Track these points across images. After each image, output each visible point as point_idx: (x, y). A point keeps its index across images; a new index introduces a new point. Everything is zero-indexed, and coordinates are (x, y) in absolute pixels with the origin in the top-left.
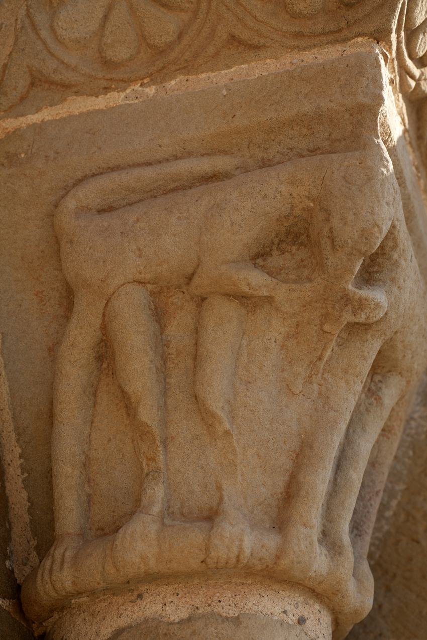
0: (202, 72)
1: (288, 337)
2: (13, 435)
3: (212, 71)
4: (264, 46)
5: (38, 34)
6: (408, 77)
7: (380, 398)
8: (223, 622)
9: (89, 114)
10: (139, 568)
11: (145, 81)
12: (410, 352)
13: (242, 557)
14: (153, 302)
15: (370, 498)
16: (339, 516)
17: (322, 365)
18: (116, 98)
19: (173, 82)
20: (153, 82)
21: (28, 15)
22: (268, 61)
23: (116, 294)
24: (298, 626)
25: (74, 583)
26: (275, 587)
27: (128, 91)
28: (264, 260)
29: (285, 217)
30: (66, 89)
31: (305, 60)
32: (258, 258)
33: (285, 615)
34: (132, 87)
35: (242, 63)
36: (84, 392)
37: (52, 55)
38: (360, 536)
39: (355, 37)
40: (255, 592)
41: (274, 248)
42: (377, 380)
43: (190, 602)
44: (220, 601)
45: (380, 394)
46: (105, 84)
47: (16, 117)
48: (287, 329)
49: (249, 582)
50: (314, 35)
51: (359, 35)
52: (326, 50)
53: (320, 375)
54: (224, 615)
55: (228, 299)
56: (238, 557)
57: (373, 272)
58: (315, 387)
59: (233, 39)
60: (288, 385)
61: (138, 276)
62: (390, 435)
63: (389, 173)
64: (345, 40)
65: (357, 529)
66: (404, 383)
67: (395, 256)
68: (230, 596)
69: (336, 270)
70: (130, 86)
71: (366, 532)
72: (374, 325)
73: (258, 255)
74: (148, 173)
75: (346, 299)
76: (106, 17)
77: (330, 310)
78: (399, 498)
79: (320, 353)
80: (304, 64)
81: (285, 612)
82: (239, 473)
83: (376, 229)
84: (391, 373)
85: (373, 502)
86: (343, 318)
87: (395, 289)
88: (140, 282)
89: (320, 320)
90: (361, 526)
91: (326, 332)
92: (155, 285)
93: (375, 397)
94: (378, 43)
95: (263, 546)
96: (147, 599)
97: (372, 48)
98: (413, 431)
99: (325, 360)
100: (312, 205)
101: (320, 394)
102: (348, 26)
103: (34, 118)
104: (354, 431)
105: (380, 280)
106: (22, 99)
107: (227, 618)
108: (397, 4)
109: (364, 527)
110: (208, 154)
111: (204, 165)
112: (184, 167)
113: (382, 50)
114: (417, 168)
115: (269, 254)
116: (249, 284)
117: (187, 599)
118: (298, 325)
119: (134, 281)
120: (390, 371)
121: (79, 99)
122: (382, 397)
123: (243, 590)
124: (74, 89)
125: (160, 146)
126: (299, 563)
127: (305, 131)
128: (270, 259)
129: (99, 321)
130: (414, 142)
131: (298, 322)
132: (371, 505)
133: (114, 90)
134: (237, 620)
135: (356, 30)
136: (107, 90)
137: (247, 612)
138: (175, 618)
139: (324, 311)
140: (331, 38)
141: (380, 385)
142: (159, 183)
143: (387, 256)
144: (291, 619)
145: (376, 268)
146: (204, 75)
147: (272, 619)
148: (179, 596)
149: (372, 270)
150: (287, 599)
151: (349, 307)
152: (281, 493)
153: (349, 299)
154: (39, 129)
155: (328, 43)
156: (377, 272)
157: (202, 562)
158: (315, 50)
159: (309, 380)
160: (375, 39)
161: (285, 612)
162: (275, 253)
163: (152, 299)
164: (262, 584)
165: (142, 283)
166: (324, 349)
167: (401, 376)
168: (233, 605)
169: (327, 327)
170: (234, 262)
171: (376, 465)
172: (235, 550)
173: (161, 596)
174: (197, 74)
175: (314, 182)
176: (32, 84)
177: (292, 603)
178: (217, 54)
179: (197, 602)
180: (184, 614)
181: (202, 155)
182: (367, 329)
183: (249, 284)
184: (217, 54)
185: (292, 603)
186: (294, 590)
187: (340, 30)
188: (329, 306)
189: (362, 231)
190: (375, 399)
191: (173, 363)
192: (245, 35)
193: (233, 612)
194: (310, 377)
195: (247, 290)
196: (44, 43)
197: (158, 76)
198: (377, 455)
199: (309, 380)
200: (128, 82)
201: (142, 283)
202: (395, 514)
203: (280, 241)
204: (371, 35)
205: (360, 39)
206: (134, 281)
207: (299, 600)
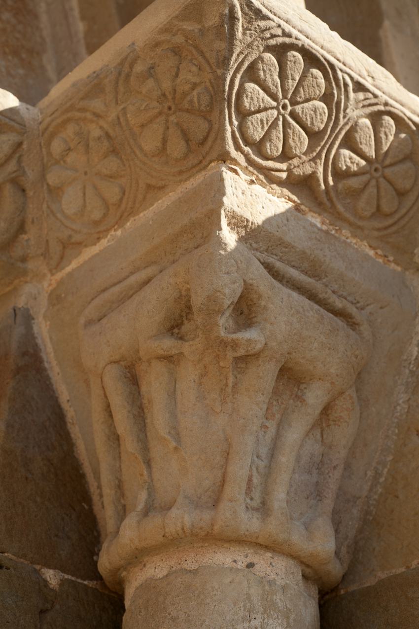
0: (141, 213)
1: (202, 376)
2: (92, 475)
3: (145, 210)
4: (165, 185)
6: (273, 173)
7: (305, 401)
8: (187, 573)
9: (90, 259)
10: (131, 547)
11: (116, 227)
13: (185, 529)
14: (128, 372)
15: (329, 472)
17: (229, 389)
18: (104, 243)
19: (128, 224)
20: (120, 227)
21: (48, 207)
22: (170, 194)
23: (104, 373)
24: (247, 569)
25: (110, 563)
26: (226, 545)
27: (109, 236)
28: (179, 329)
29: (178, 298)
30: (80, 245)
31: (188, 188)
32: (174, 328)
34: (110, 233)
35: (158, 201)
36: (109, 439)
37: (67, 227)
38: (321, 500)
39: (209, 164)
40: (211, 551)
41: (184, 319)
42: (303, 388)
43: (169, 564)
44: (186, 561)
45: (304, 397)
48: (199, 371)
49: (206, 545)
50: (188, 170)
51: (211, 162)
52: (197, 177)
54: (189, 569)
55: (160, 361)
56: (183, 529)
59: (149, 187)
60: (212, 408)
62: (339, 424)
63: (227, 253)
64: (205, 167)
65: (319, 496)
67: (263, 303)
68: (193, 556)
69: (205, 327)
70: (109, 233)
73: (173, 327)
74: (116, 289)
75: (224, 344)
76: (84, 194)
78: (388, 466)
79: (225, 382)
80: (187, 190)
81: (235, 561)
83: (218, 294)
84: (313, 380)
86: (228, 356)
87: (268, 325)
88: (115, 362)
89: (217, 360)
91: (223, 367)
92: (126, 362)
93: (300, 400)
94: (225, 162)
95: (201, 520)
96: (148, 566)
97: (219, 167)
98: (399, 414)
102: (204, 158)
103: (69, 269)
104: (283, 428)
105: (257, 322)
106: (62, 258)
107: (190, 571)
108: (224, 135)
110: (147, 267)
111: (142, 275)
112: (133, 279)
113: (228, 166)
115: (182, 323)
116: (162, 349)
117: (167, 562)
118: (205, 367)
119: (111, 362)
120: (311, 379)
121: (87, 249)
122: (306, 399)
123: (203, 551)
125: (122, 269)
126: (227, 526)
127: (190, 236)
128: (183, 327)
131: (204, 365)
132: (330, 477)
133: (102, 238)
134: (195, 572)
135: (208, 159)
136: (99, 239)
137: (205, 564)
138: (160, 576)
139: (215, 354)
140: (197, 168)
141: (305, 391)
142: (124, 293)
143: (257, 305)
144: (241, 565)
145: (253, 315)
146: (142, 215)
148: (164, 561)
149: (251, 316)
150: (237, 552)
151: (229, 348)
152: (221, 482)
154: (70, 275)
155: (197, 172)
156: (255, 317)
157: (164, 536)
158: (192, 180)
160: (222, 160)
161: (235, 561)
162: (186, 322)
163: (128, 370)
164: (216, 545)
165: (117, 362)
167: (322, 380)
168: (195, 562)
169: (222, 364)
170: (154, 336)
171: (332, 447)
172: (179, 524)
173: (154, 563)
174: (138, 215)
175: (185, 271)
176: (64, 247)
177: (242, 554)
178: (144, 198)
179: (172, 563)
180: (165, 573)
181: (145, 268)
182: (257, 358)
183: (162, 349)
184: (144, 198)
185: (242, 554)
186: (243, 546)
187: (201, 162)
189: (208, 297)
190: (301, 402)
191: (148, 409)
192: (153, 182)
193: (194, 566)
195: (163, 353)
196: (61, 221)
197: (120, 222)
198: (332, 440)
200: (107, 231)
201: (117, 362)
202: (386, 479)
203: (187, 313)
204: (218, 160)
205: (213, 164)
206: (111, 362)
207: (249, 552)
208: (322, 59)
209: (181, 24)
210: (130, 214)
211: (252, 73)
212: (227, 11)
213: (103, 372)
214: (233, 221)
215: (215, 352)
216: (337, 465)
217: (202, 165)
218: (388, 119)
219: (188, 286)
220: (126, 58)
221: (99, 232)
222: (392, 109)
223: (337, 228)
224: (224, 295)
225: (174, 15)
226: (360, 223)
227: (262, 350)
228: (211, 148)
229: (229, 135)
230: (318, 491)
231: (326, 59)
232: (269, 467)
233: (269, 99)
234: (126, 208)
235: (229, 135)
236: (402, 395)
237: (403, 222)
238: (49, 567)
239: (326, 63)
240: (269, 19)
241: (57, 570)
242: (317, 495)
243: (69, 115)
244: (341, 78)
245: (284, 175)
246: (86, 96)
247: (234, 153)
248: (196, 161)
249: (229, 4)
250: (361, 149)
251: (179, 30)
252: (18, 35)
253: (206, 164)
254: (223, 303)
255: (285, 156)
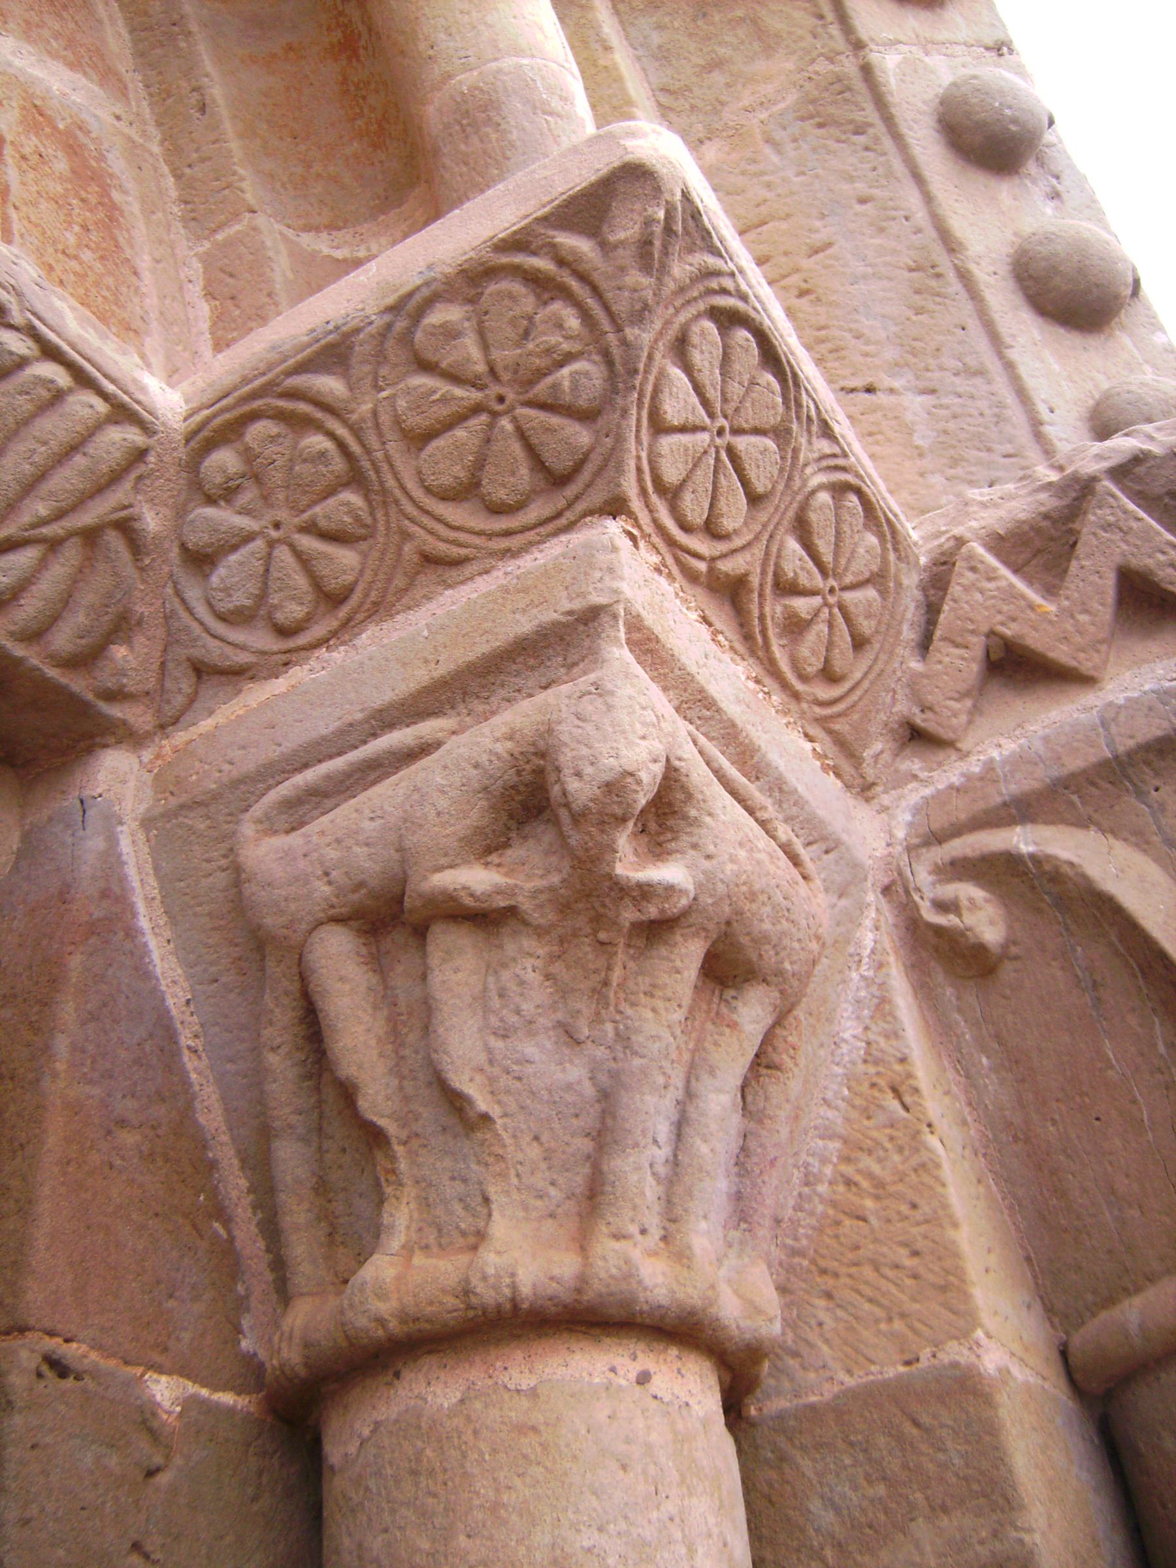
5: (192, 614)
12: (767, 947)
16: (686, 1211)
24: (638, 1388)
33: (612, 1375)
46: (284, 658)
47: (186, 729)
53: (612, 1008)
57: (665, 842)
58: (609, 1027)
59: (430, 560)
61: (332, 912)
66: (777, 994)
71: (759, 1224)
72: (682, 919)
77: (601, 910)
82: (512, 1172)
85: (766, 1178)
90: (751, 1216)
99: (615, 984)
100: (542, 762)
101: (617, 1034)
109: (755, 1218)
114: (757, 681)
116: (472, 895)
124: (250, 674)
129: (297, 985)
130: (738, 646)
132: (764, 1182)
134: (533, 1393)
135: (580, 507)
139: (592, 912)
140: (550, 527)
147: (590, 1384)
153: (622, 889)
154: (208, 737)
159: (597, 1019)
166: (609, 968)
187: (559, 515)
188: (597, 905)
192: (442, 548)
194: (598, 1014)
195: (473, 904)
199: (597, 1019)
208: (784, 360)
209: (551, 233)
210: (369, 617)
211: (681, 347)
212: (661, 214)
213: (306, 941)
214: (636, 636)
215: (593, 908)
216: (776, 1159)
217: (563, 521)
218: (853, 500)
219: (542, 762)
220: (410, 295)
221: (289, 651)
222: (865, 488)
223: (766, 689)
224: (639, 782)
225: (540, 213)
226: (799, 686)
227: (686, 913)
228: (588, 486)
229: (632, 464)
230: (742, 1211)
231: (788, 362)
232: (675, 1162)
233: (703, 412)
234: (362, 604)
235: (632, 464)
236: (849, 1024)
237: (854, 697)
238: (160, 1370)
239: (788, 369)
240: (721, 256)
241: (175, 1377)
242: (740, 1220)
243: (257, 404)
244: (805, 404)
245: (702, 566)
246: (302, 368)
247: (636, 504)
248: (547, 512)
249: (667, 202)
250: (816, 545)
251: (544, 246)
252: (107, 294)
253: (573, 519)
254: (635, 802)
255: (711, 530)
